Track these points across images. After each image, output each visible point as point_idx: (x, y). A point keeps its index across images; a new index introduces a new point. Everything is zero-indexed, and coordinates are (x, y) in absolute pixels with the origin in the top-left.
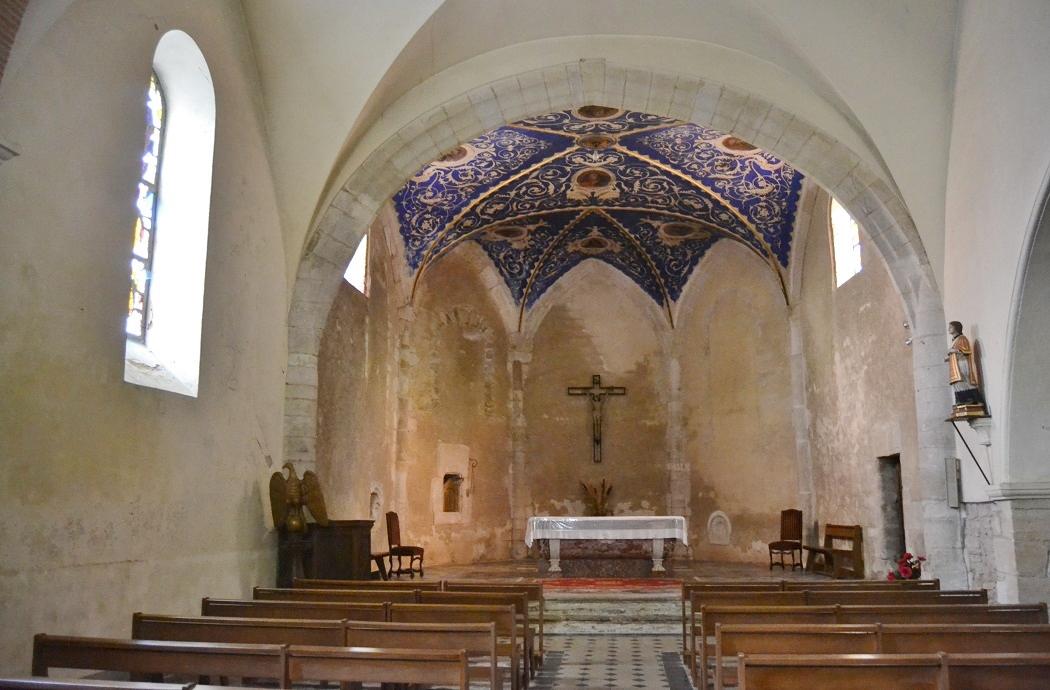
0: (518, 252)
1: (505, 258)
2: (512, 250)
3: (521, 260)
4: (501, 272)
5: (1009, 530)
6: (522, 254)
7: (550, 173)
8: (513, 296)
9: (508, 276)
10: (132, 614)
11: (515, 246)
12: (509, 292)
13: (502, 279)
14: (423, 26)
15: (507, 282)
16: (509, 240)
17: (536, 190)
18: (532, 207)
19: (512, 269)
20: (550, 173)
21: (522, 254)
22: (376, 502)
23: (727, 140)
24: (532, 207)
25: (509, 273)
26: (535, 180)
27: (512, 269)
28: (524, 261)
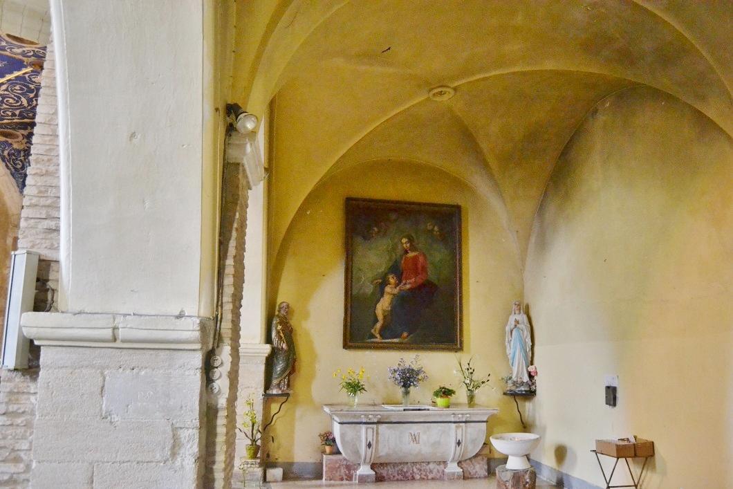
0: (19, 151)
1: (9, 154)
2: (13, 149)
3: (22, 158)
4: (7, 166)
5: (596, 72)
6: (22, 154)
7: (18, 87)
8: (18, 187)
9: (13, 170)
10: (617, 407)
11: (15, 146)
12: (15, 184)
13: (9, 172)
14: (606, 397)
15: (13, 175)
16: (10, 141)
17: (11, 101)
18: (14, 115)
19: (16, 164)
20: (18, 87)
21: (22, 154)
22: (210, 386)
23: (619, 402)
24: (14, 115)
25: (14, 168)
26: (6, 92)
27: (16, 164)
28: (25, 159)
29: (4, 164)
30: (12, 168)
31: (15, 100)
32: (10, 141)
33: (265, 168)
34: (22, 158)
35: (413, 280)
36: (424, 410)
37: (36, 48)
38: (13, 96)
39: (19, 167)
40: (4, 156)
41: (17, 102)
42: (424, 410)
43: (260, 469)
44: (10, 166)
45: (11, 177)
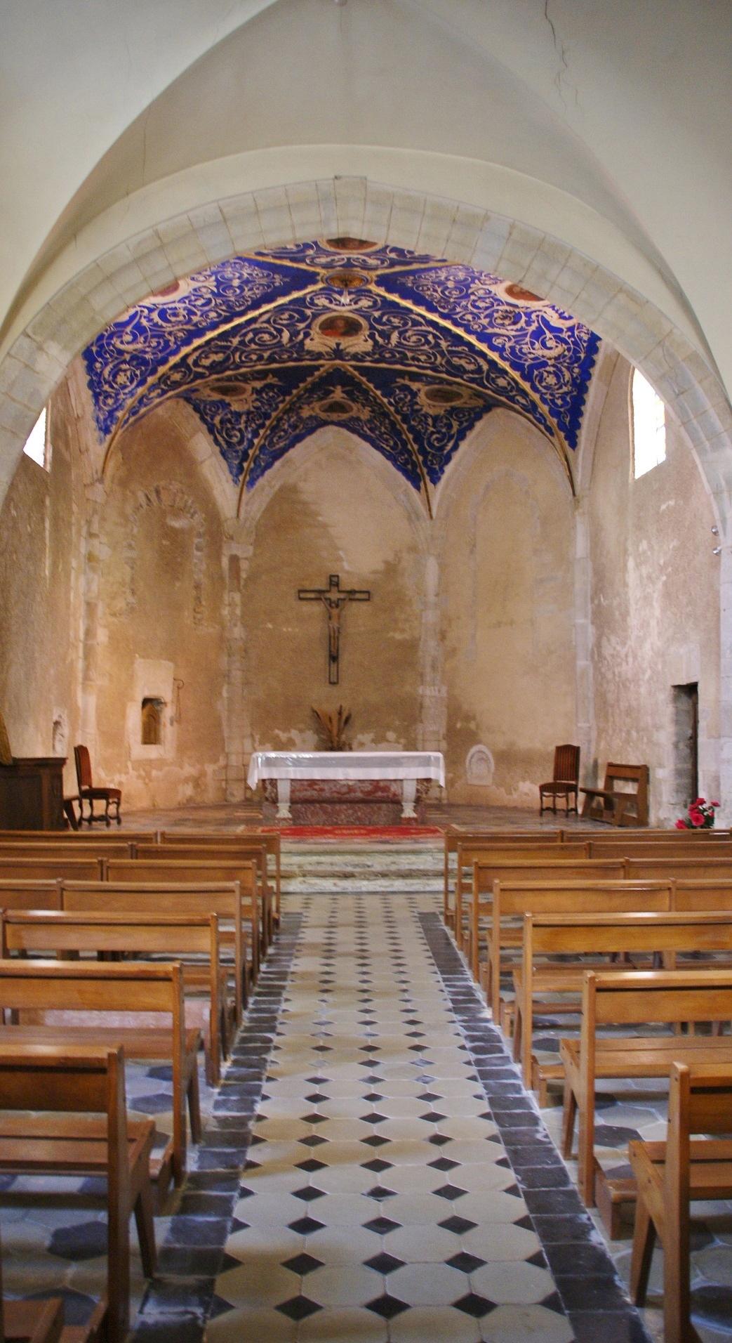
0: (238, 415)
1: (222, 422)
2: (231, 412)
3: (242, 426)
4: (216, 441)
6: (244, 418)
11: (235, 407)
13: (217, 449)
15: (223, 454)
16: (227, 399)
17: (266, 337)
18: (260, 358)
20: (286, 316)
21: (244, 418)
24: (260, 358)
25: (228, 443)
27: (230, 437)
29: (212, 437)
30: (223, 443)
31: (271, 334)
32: (227, 399)
33: (600, 339)
34: (242, 426)
35: (663, 507)
36: (135, 955)
37: (368, 255)
38: (272, 330)
39: (235, 440)
40: (214, 425)
41: (275, 337)
42: (135, 955)
43: (105, 1056)
44: (220, 439)
45: (221, 458)
